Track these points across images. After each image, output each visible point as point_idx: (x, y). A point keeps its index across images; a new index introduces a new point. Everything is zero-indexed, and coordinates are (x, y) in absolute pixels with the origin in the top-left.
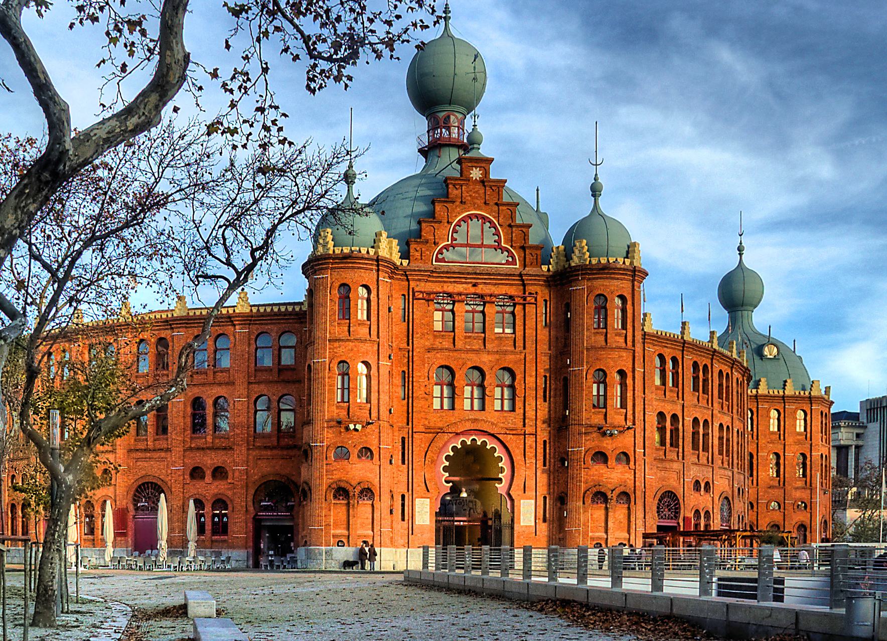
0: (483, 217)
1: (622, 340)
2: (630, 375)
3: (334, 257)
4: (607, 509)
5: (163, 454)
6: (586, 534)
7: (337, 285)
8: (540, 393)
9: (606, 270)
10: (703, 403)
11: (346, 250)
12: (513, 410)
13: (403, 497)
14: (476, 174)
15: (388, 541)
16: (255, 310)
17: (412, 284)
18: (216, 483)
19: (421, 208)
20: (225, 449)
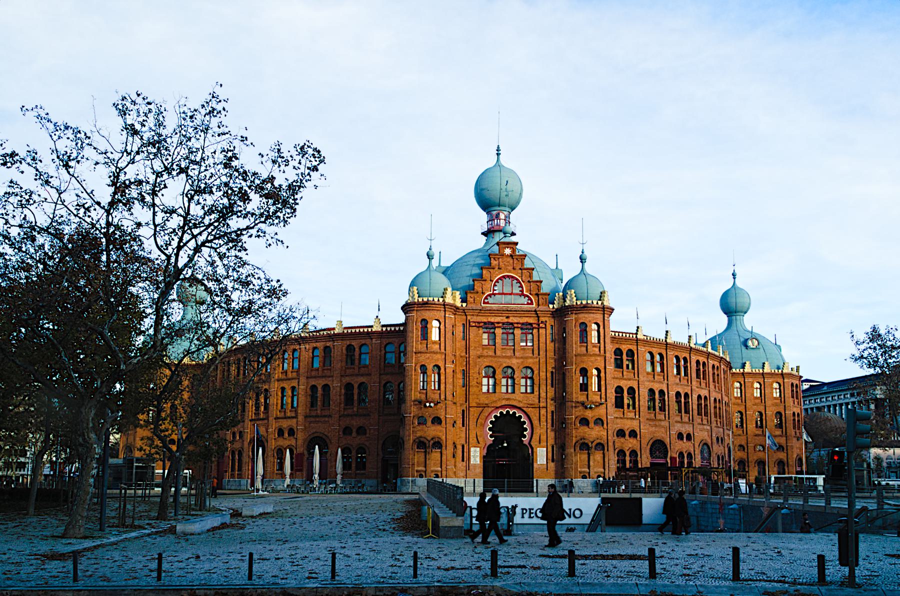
0: (512, 277)
1: (597, 350)
2: (603, 371)
3: (418, 304)
4: (589, 454)
6: (576, 469)
7: (420, 320)
8: (549, 381)
9: (585, 308)
11: (425, 299)
12: (533, 392)
13: (463, 446)
14: (508, 251)
16: (384, 329)
17: (469, 318)
19: (477, 271)
20: (365, 415)
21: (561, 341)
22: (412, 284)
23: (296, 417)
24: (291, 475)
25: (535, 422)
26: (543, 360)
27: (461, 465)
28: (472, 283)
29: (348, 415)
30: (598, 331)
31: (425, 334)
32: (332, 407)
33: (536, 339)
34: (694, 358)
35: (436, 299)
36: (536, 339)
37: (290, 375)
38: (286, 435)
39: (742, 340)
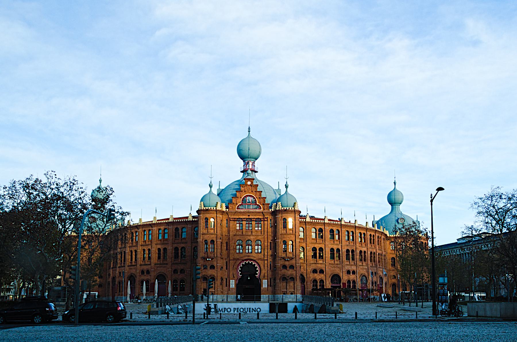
3: (204, 210)
8: (269, 247)
11: (207, 208)
13: (226, 279)
14: (249, 183)
15: (220, 292)
19: (234, 192)
21: (275, 227)
22: (201, 201)
23: (150, 264)
24: (146, 294)
25: (262, 267)
26: (266, 237)
27: (225, 288)
29: (176, 264)
32: (168, 260)
33: (263, 226)
35: (212, 208)
36: (263, 226)
37: (147, 243)
38: (145, 274)
39: (397, 218)
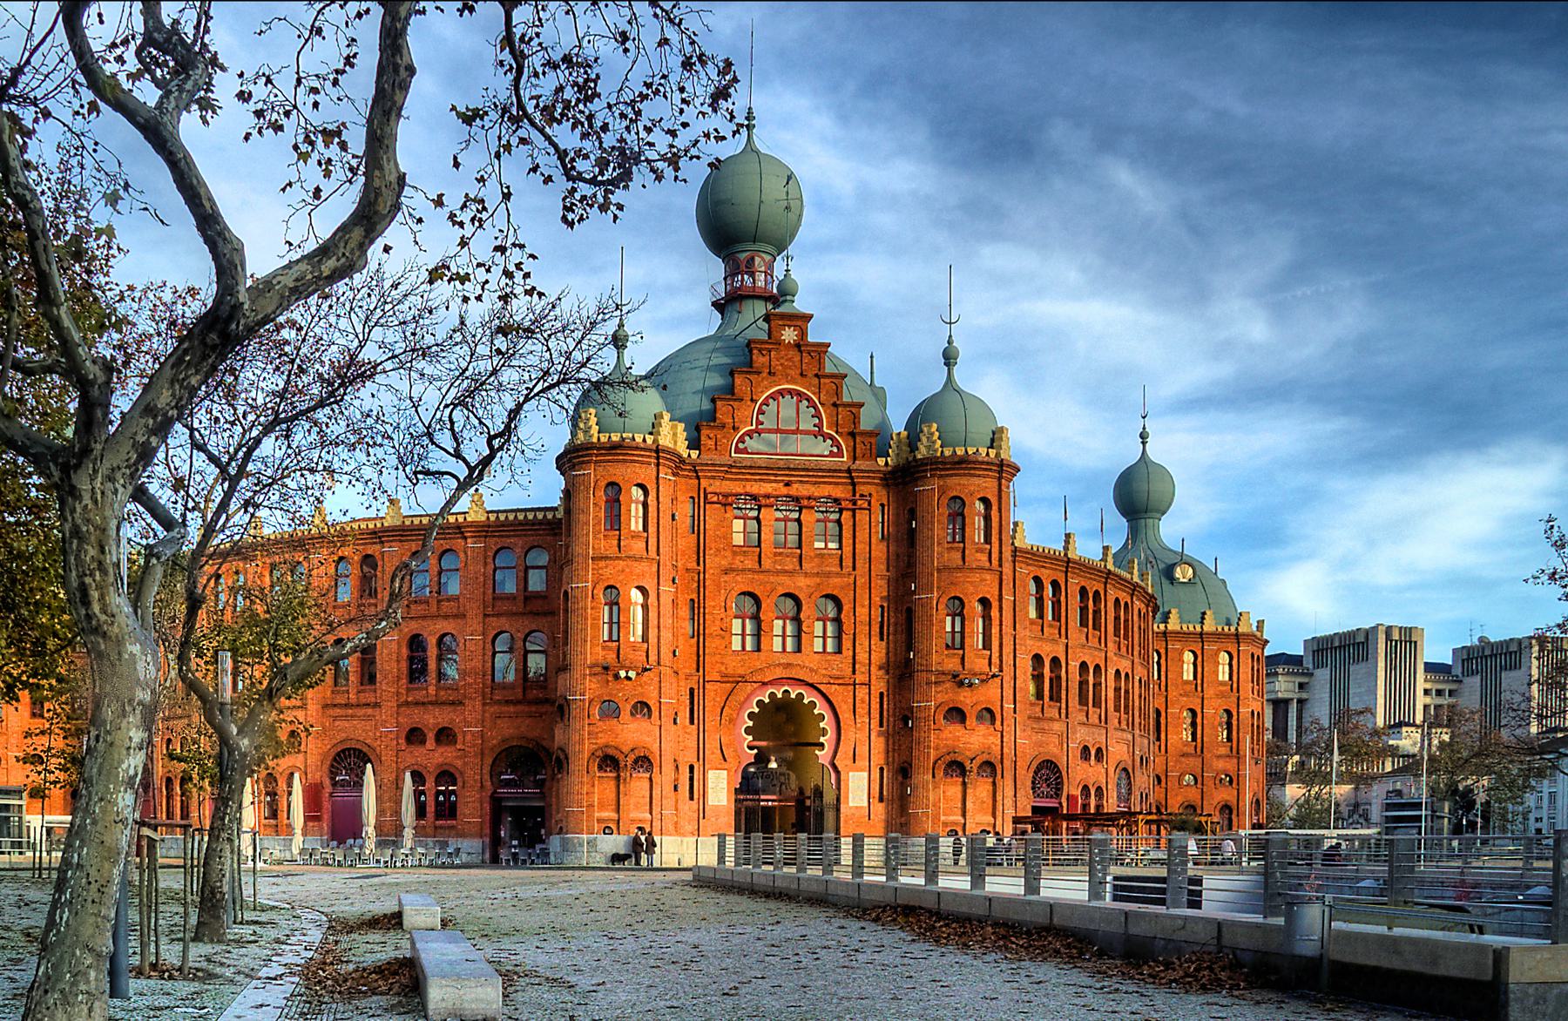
0: (799, 394)
1: (985, 558)
2: (995, 604)
3: (600, 447)
4: (964, 784)
5: (370, 711)
6: (936, 818)
7: (603, 484)
8: (876, 629)
9: (963, 464)
10: (1093, 642)
11: (615, 438)
12: (839, 652)
13: (692, 768)
14: (789, 335)
16: (492, 517)
17: (704, 483)
18: (441, 750)
19: (715, 380)
20: (453, 703)
25: (845, 716)
27: (688, 808)
28: (706, 405)
30: (987, 518)
31: (615, 518)
34: (1075, 583)
35: (639, 438)
39: (1162, 566)
